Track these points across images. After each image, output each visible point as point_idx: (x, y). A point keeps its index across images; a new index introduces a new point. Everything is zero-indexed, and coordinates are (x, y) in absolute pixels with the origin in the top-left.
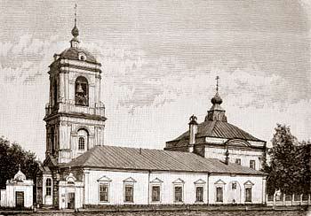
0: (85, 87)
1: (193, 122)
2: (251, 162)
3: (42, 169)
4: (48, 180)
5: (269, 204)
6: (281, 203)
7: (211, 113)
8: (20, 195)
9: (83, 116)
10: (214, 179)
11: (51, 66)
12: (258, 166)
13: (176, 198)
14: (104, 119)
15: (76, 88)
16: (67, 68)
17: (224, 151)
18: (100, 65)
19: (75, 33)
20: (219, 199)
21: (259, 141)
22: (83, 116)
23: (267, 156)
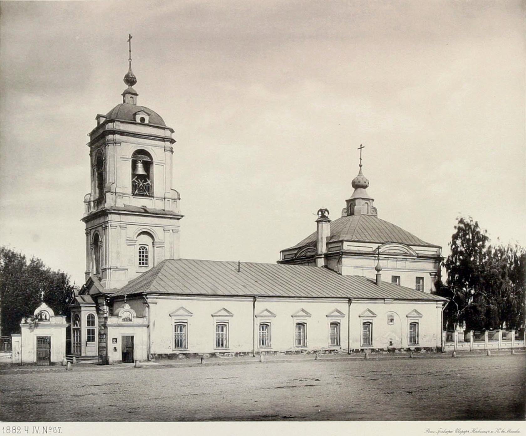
0: (148, 165)
1: (323, 217)
2: (419, 279)
3: (79, 299)
4: (90, 318)
5: (448, 347)
6: (466, 346)
7: (351, 203)
8: (44, 342)
9: (145, 212)
10: (359, 308)
11: (92, 134)
12: (429, 285)
13: (299, 341)
14: (172, 141)
15: (134, 167)
16: (117, 137)
17: (373, 263)
18: (172, 131)
19: (130, 80)
20: (368, 339)
21: (433, 246)
22: (145, 212)
23: (463, 295)
